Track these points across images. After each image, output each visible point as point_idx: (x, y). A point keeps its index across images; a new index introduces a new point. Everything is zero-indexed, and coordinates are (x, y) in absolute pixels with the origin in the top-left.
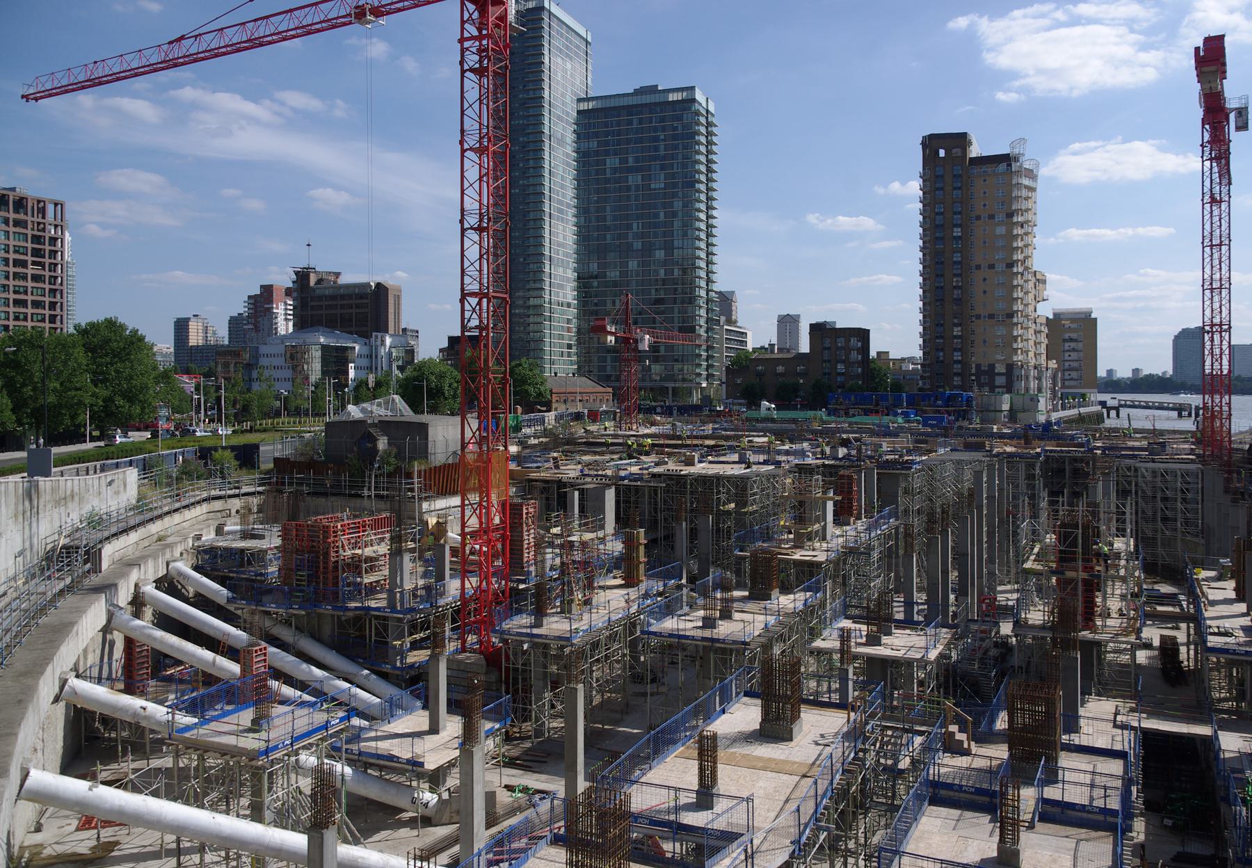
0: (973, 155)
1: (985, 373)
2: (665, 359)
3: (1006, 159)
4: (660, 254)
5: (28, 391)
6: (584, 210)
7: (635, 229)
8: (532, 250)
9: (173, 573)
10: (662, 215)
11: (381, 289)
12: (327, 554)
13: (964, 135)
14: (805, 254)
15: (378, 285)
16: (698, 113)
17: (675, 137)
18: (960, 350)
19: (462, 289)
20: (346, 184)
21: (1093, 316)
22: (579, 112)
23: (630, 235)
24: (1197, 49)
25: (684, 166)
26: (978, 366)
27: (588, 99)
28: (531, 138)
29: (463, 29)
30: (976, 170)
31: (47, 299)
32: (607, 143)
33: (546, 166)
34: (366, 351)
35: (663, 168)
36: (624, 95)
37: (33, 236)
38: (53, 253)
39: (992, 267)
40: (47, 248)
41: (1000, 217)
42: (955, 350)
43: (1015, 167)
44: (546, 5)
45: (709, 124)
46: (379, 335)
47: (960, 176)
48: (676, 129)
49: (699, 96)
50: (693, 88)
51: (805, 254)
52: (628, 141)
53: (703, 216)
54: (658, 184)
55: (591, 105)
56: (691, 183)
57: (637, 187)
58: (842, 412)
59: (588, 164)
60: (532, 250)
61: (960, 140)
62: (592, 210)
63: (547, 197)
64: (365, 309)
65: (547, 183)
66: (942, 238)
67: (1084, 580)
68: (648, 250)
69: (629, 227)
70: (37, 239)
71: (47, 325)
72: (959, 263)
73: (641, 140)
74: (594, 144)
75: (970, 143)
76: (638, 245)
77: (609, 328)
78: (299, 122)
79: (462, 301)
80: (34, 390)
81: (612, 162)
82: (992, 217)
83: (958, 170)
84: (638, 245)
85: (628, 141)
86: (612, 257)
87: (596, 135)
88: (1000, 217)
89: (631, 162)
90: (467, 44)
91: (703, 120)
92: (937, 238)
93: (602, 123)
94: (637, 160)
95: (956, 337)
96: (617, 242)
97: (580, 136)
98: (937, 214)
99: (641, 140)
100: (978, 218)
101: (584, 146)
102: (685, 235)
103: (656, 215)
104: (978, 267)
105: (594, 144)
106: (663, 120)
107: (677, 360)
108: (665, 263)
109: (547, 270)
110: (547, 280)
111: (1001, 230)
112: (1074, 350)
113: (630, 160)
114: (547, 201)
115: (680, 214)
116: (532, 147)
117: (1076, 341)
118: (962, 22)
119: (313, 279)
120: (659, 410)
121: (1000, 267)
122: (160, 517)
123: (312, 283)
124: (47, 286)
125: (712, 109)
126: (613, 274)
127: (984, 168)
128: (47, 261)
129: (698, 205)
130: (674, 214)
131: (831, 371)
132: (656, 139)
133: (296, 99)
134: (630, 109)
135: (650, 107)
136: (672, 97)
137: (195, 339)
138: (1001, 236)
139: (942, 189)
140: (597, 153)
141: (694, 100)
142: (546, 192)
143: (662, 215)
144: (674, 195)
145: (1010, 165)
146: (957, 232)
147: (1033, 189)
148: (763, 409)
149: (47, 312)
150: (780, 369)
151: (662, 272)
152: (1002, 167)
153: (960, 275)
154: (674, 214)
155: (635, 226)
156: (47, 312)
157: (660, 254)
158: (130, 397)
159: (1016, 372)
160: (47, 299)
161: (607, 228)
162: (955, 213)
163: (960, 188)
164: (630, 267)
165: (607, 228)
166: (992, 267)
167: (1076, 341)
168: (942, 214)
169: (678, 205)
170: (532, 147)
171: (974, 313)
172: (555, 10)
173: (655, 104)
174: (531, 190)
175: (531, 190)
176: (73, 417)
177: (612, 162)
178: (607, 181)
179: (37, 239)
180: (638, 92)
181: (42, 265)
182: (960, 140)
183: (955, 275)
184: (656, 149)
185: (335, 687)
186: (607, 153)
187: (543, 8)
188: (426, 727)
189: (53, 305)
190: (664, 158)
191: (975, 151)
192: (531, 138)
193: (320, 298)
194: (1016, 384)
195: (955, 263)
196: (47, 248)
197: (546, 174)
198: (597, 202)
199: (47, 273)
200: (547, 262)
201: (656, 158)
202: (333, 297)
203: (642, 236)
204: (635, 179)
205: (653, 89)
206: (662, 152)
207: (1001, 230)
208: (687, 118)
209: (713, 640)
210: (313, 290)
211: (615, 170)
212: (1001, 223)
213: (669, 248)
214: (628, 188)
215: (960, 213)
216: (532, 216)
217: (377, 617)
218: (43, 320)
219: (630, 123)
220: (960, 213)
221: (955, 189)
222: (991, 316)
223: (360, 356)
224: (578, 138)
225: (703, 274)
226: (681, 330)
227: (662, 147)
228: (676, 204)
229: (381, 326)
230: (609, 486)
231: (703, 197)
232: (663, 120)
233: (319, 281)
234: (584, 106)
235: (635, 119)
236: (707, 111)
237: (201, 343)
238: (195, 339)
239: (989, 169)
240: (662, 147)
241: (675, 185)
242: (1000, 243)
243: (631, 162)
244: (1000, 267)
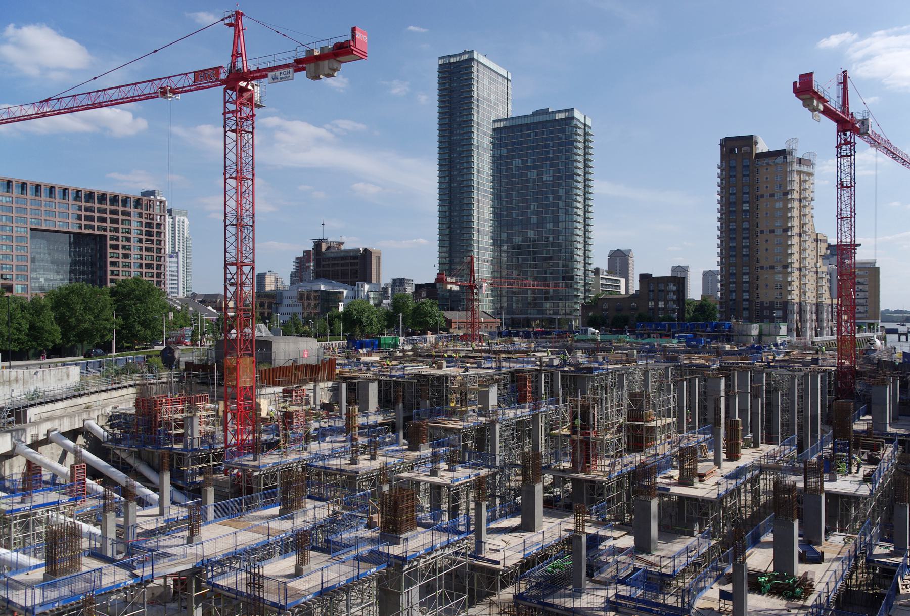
0: (759, 151)
1: (767, 308)
2: (552, 299)
3: (782, 153)
4: (549, 226)
5: (73, 321)
6: (498, 196)
7: (532, 209)
8: (465, 225)
9: (87, 426)
10: (551, 198)
11: (367, 253)
12: (156, 416)
13: (751, 137)
14: (652, 222)
15: (365, 250)
16: (576, 127)
17: (560, 144)
18: (748, 291)
19: (225, 261)
20: (361, 182)
21: (877, 265)
22: (494, 130)
23: (529, 213)
24: (795, 83)
25: (566, 164)
26: (762, 303)
27: (501, 120)
28: (465, 148)
29: (225, 107)
30: (761, 162)
31: (155, 263)
32: (513, 150)
33: (475, 166)
34: (352, 294)
35: (552, 166)
36: (525, 116)
37: (146, 223)
38: (159, 234)
39: (772, 231)
40: (155, 230)
41: (778, 195)
42: (744, 291)
43: (789, 159)
44: (475, 56)
45: (586, 134)
46: (360, 283)
47: (748, 166)
48: (561, 138)
49: (577, 114)
50: (572, 110)
51: (652, 222)
52: (528, 148)
53: (580, 199)
54: (548, 177)
55: (502, 124)
56: (571, 176)
57: (534, 179)
58: (645, 336)
59: (498, 162)
60: (465, 225)
61: (749, 140)
62: (503, 196)
63: (476, 188)
64: (358, 266)
65: (475, 178)
66: (734, 212)
67: (581, 441)
68: (541, 223)
69: (528, 208)
70: (149, 225)
71: (155, 279)
72: (748, 229)
73: (536, 147)
74: (504, 151)
75: (756, 143)
76: (534, 220)
77: (449, 279)
78: (347, 140)
79: (226, 267)
80: (77, 320)
81: (517, 163)
82: (772, 195)
83: (746, 162)
84: (534, 220)
85: (528, 148)
86: (516, 229)
87: (506, 145)
88: (778, 195)
89: (529, 163)
90: (228, 116)
91: (580, 132)
92: (731, 212)
93: (509, 135)
94: (534, 161)
95: (745, 282)
96: (520, 218)
97: (496, 146)
98: (731, 194)
99: (536, 147)
100: (762, 196)
101: (498, 152)
102: (567, 212)
103: (547, 199)
104: (762, 232)
105: (504, 151)
106: (551, 132)
107: (561, 300)
108: (553, 232)
109: (475, 238)
110: (476, 245)
111: (779, 205)
112: (861, 291)
113: (529, 161)
114: (475, 191)
115: (563, 198)
116: (465, 154)
117: (862, 284)
118: (834, 41)
119: (324, 247)
120: (521, 334)
121: (779, 232)
122: (88, 394)
123: (323, 250)
124: (155, 255)
125: (589, 123)
126: (517, 240)
127: (767, 160)
128: (155, 238)
129: (576, 191)
130: (559, 198)
131: (655, 310)
132: (547, 146)
133: (346, 125)
134: (529, 126)
135: (544, 124)
136: (558, 116)
137: (270, 286)
138: (779, 209)
139: (735, 176)
140: (507, 157)
141: (573, 118)
142: (475, 184)
143: (551, 198)
144: (560, 185)
145: (785, 158)
146: (746, 207)
147: (811, 174)
148: (589, 333)
149: (155, 271)
150: (606, 306)
151: (551, 239)
152: (780, 159)
153: (748, 238)
154: (559, 198)
155: (532, 206)
156: (155, 271)
157: (549, 226)
158: (145, 324)
159: (789, 308)
160: (155, 263)
161: (513, 209)
162: (744, 193)
163: (748, 175)
164: (529, 235)
165: (513, 209)
166: (772, 231)
167: (862, 284)
168: (734, 194)
169: (562, 191)
170: (465, 154)
171: (759, 265)
172: (482, 59)
173: (546, 122)
174: (464, 183)
175: (464, 183)
176: (103, 337)
177: (517, 163)
178: (513, 176)
179: (149, 225)
180: (536, 114)
181: (152, 241)
182: (749, 140)
183: (744, 238)
184: (547, 153)
185: (142, 492)
186: (513, 157)
187: (472, 59)
188: (158, 513)
189: (159, 267)
190: (553, 159)
191: (762, 147)
192: (465, 148)
193: (329, 259)
194: (789, 316)
195: (744, 229)
196: (155, 230)
197: (475, 172)
198: (506, 191)
199: (155, 246)
200: (476, 234)
201: (547, 159)
202: (335, 259)
203: (538, 213)
204: (532, 175)
205: (545, 112)
206: (551, 155)
207: (779, 205)
208: (568, 130)
209: (325, 468)
210: (324, 254)
211: (519, 168)
212: (779, 200)
213: (556, 221)
214: (527, 181)
215: (748, 193)
216: (465, 201)
217: (177, 454)
218: (152, 276)
219: (529, 135)
220: (748, 193)
221: (744, 176)
222: (772, 267)
223: (347, 297)
224: (494, 147)
225: (581, 239)
226: (564, 278)
227: (551, 152)
228: (560, 191)
229: (366, 277)
230: (373, 381)
231: (581, 186)
232: (551, 132)
233: (328, 248)
234: (497, 125)
235: (532, 133)
236: (585, 125)
237: (273, 289)
238: (270, 286)
239: (770, 161)
240: (551, 152)
241: (560, 178)
242: (778, 214)
243: (529, 163)
244: (779, 232)
